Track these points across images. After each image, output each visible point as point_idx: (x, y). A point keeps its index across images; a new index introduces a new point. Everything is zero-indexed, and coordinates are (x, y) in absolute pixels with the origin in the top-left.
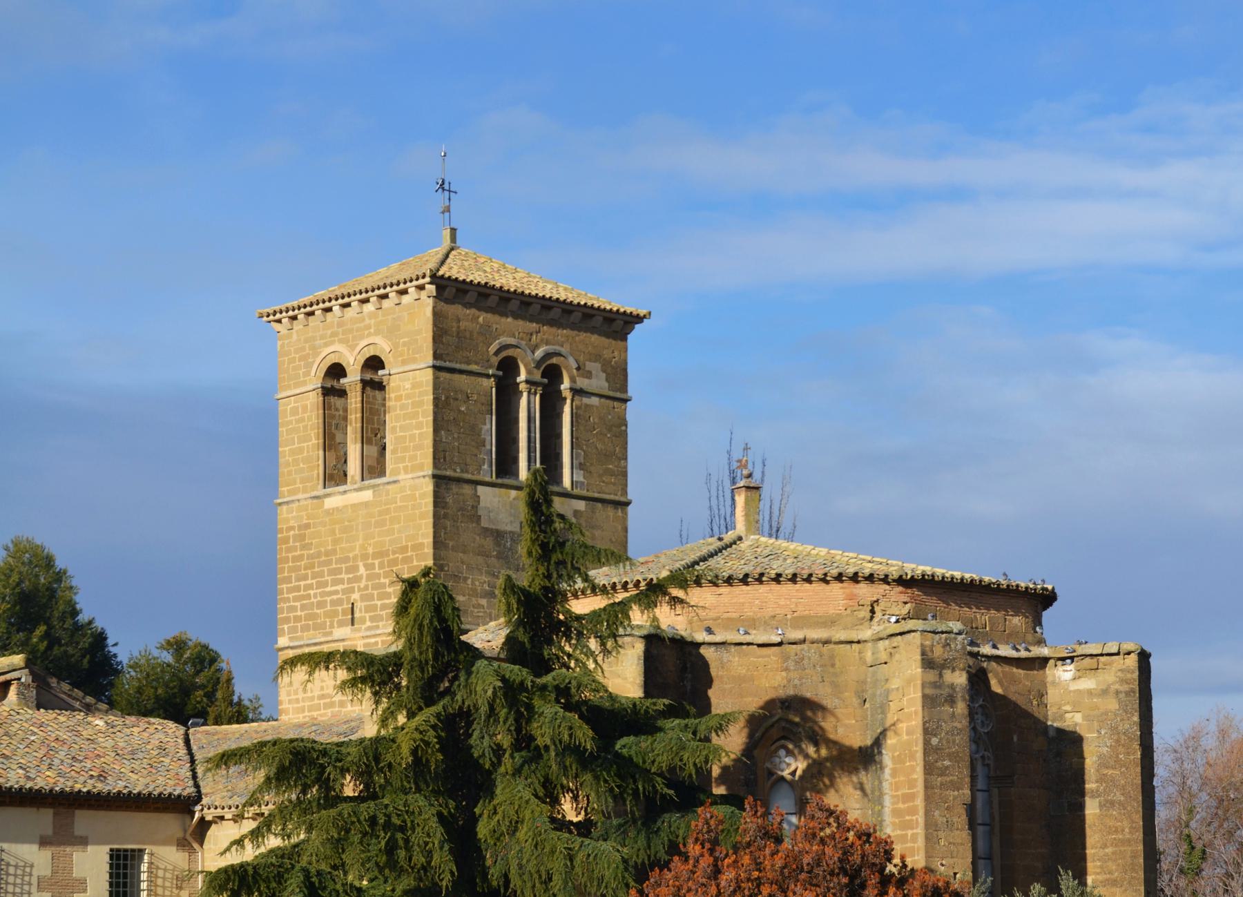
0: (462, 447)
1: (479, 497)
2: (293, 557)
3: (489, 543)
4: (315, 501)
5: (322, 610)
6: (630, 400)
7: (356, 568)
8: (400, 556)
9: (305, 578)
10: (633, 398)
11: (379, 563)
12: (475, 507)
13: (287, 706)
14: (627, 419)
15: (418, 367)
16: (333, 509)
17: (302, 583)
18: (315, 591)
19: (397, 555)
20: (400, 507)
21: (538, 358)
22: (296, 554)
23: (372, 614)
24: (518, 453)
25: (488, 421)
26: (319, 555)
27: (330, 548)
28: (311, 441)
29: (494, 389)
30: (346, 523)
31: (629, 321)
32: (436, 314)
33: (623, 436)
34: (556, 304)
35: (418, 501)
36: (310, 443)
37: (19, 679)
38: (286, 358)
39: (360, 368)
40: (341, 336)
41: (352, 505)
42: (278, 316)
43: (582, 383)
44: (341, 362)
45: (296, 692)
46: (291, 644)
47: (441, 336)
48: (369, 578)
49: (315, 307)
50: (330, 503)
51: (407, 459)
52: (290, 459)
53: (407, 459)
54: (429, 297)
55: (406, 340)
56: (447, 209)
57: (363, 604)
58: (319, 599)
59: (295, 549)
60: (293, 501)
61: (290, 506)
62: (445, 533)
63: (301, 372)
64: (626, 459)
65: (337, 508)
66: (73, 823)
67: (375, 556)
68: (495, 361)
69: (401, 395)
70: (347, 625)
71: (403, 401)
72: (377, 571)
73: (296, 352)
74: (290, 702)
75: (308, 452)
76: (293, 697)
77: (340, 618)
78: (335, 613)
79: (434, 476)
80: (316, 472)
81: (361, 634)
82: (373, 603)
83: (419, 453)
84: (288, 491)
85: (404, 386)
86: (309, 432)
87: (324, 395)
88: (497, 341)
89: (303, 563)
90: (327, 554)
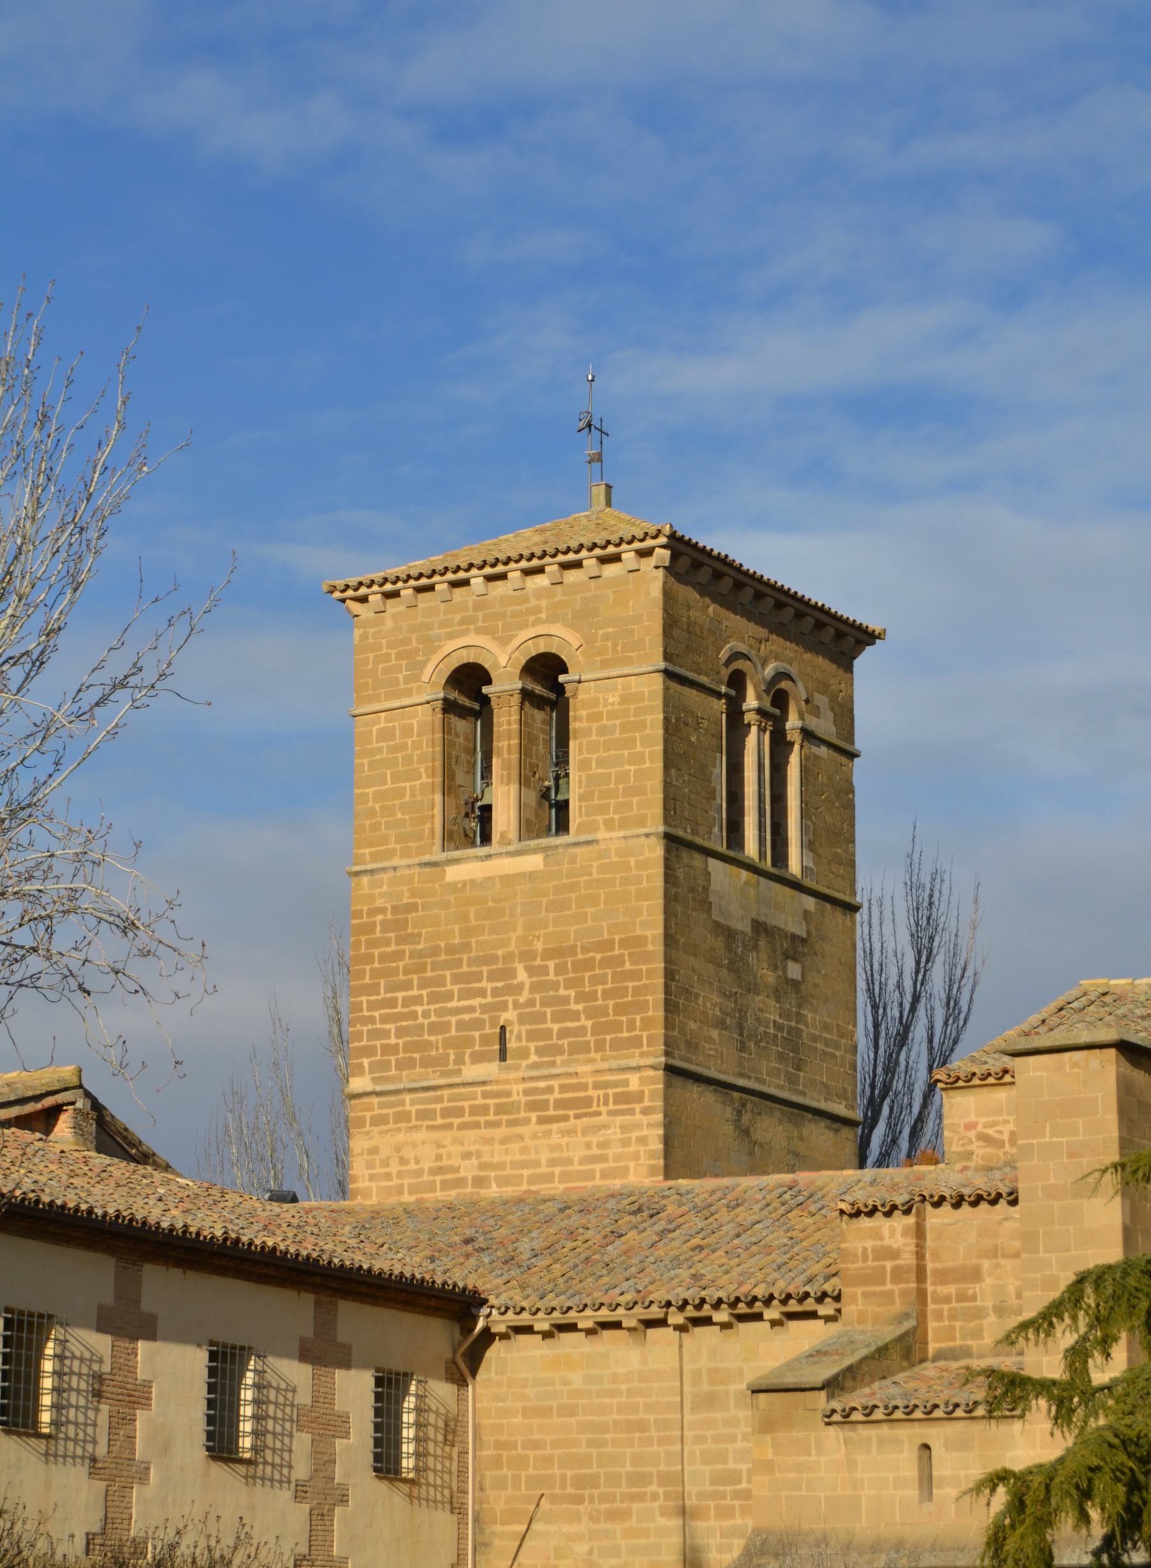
0: (693, 796)
1: (709, 874)
2: (382, 955)
3: (719, 943)
4: (427, 870)
5: (440, 1037)
6: (858, 756)
7: (511, 973)
8: (598, 956)
9: (407, 986)
10: (862, 754)
11: (556, 966)
12: (706, 889)
13: (367, 1184)
14: (855, 783)
15: (636, 671)
16: (464, 883)
17: (400, 995)
18: (426, 1007)
19: (591, 954)
20: (598, 881)
21: (769, 678)
22: (388, 949)
23: (541, 1043)
24: (743, 815)
25: (718, 761)
26: (435, 951)
27: (457, 941)
28: (419, 778)
29: (724, 716)
30: (490, 904)
31: (865, 637)
32: (667, 594)
33: (850, 806)
34: (789, 601)
35: (634, 872)
36: (418, 783)
37: (73, 1103)
38: (371, 656)
39: (518, 671)
40: (480, 624)
41: (501, 878)
42: (363, 591)
43: (813, 723)
44: (480, 662)
45: (385, 1163)
46: (378, 1088)
47: (671, 627)
48: (534, 988)
49: (437, 578)
50: (454, 873)
51: (612, 809)
52: (377, 807)
53: (612, 809)
54: (657, 567)
55: (611, 630)
56: (598, 458)
57: (524, 1028)
58: (433, 1018)
59: (387, 942)
60: (384, 869)
61: (376, 877)
62: (676, 924)
63: (401, 676)
64: (853, 842)
65: (473, 882)
66: (336, 1320)
67: (548, 954)
68: (725, 673)
69: (602, 713)
70: (490, 1060)
71: (605, 722)
72: (552, 976)
73: (390, 645)
74: (372, 1178)
75: (412, 795)
76: (379, 1170)
77: (477, 1048)
78: (468, 1042)
79: (668, 837)
80: (428, 826)
81: (521, 1074)
82: (543, 1026)
83: (635, 800)
84: (371, 854)
85: (606, 700)
86: (415, 766)
87: (445, 710)
88: (728, 646)
89: (401, 964)
90: (450, 950)
